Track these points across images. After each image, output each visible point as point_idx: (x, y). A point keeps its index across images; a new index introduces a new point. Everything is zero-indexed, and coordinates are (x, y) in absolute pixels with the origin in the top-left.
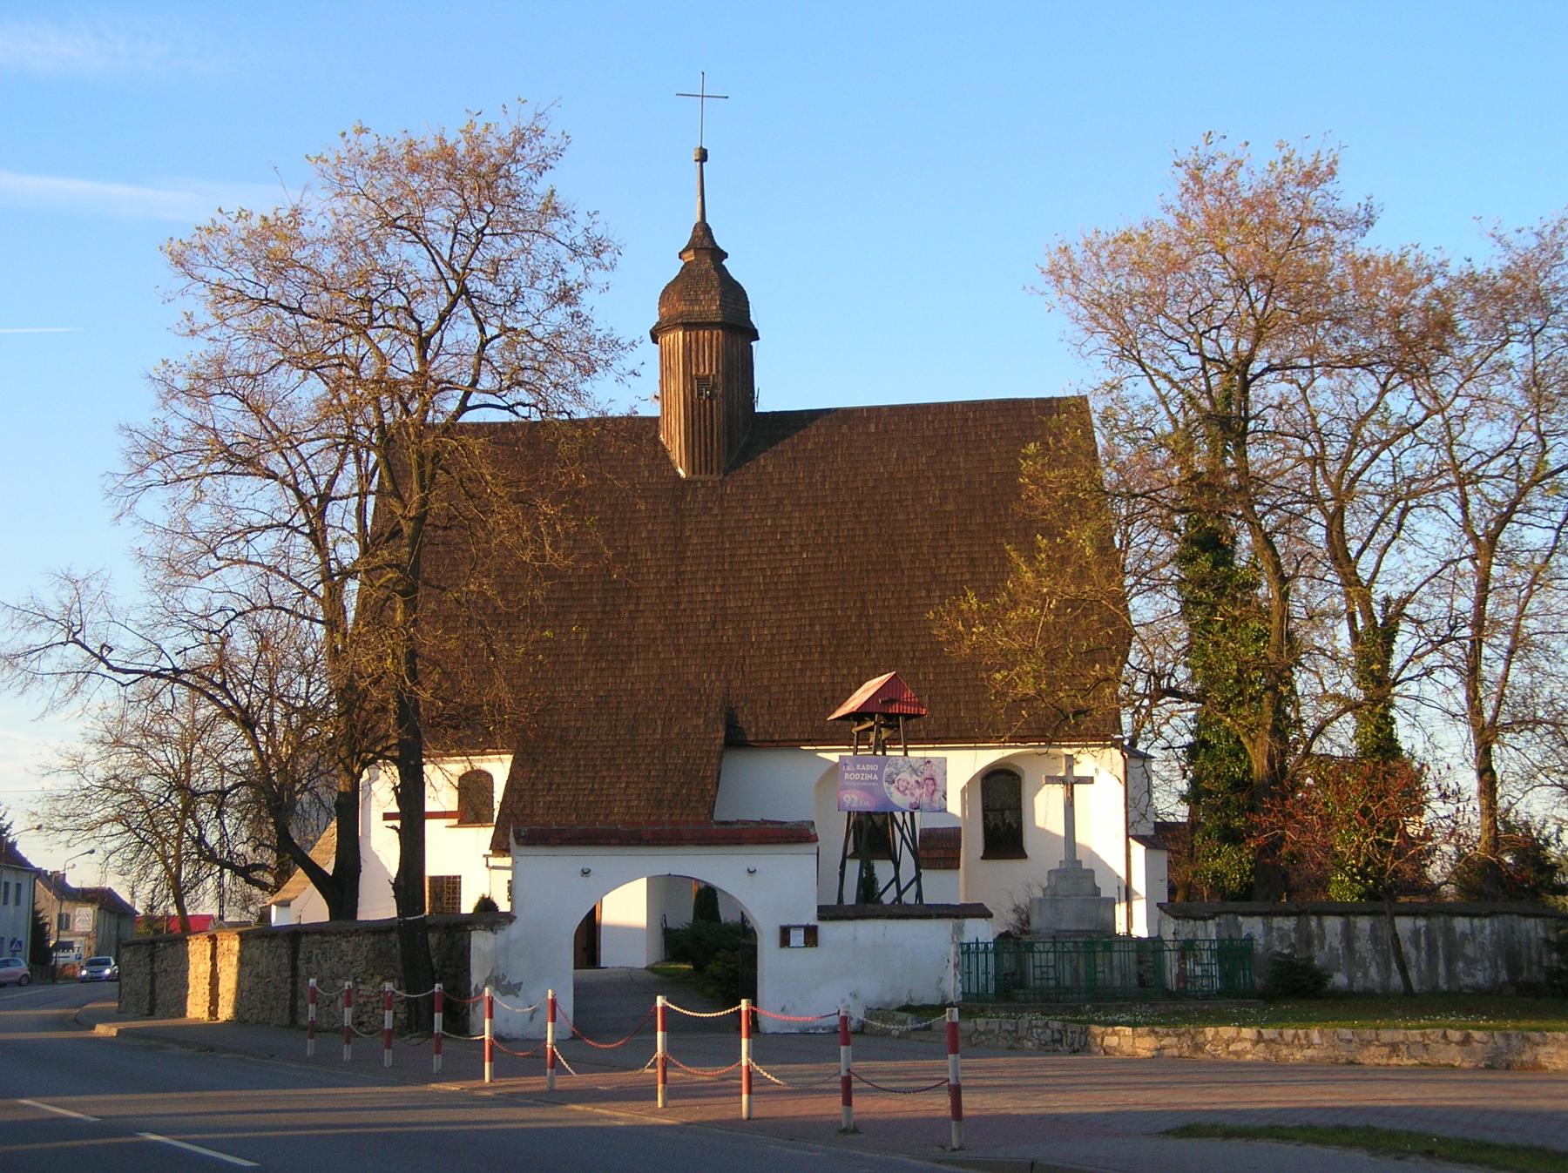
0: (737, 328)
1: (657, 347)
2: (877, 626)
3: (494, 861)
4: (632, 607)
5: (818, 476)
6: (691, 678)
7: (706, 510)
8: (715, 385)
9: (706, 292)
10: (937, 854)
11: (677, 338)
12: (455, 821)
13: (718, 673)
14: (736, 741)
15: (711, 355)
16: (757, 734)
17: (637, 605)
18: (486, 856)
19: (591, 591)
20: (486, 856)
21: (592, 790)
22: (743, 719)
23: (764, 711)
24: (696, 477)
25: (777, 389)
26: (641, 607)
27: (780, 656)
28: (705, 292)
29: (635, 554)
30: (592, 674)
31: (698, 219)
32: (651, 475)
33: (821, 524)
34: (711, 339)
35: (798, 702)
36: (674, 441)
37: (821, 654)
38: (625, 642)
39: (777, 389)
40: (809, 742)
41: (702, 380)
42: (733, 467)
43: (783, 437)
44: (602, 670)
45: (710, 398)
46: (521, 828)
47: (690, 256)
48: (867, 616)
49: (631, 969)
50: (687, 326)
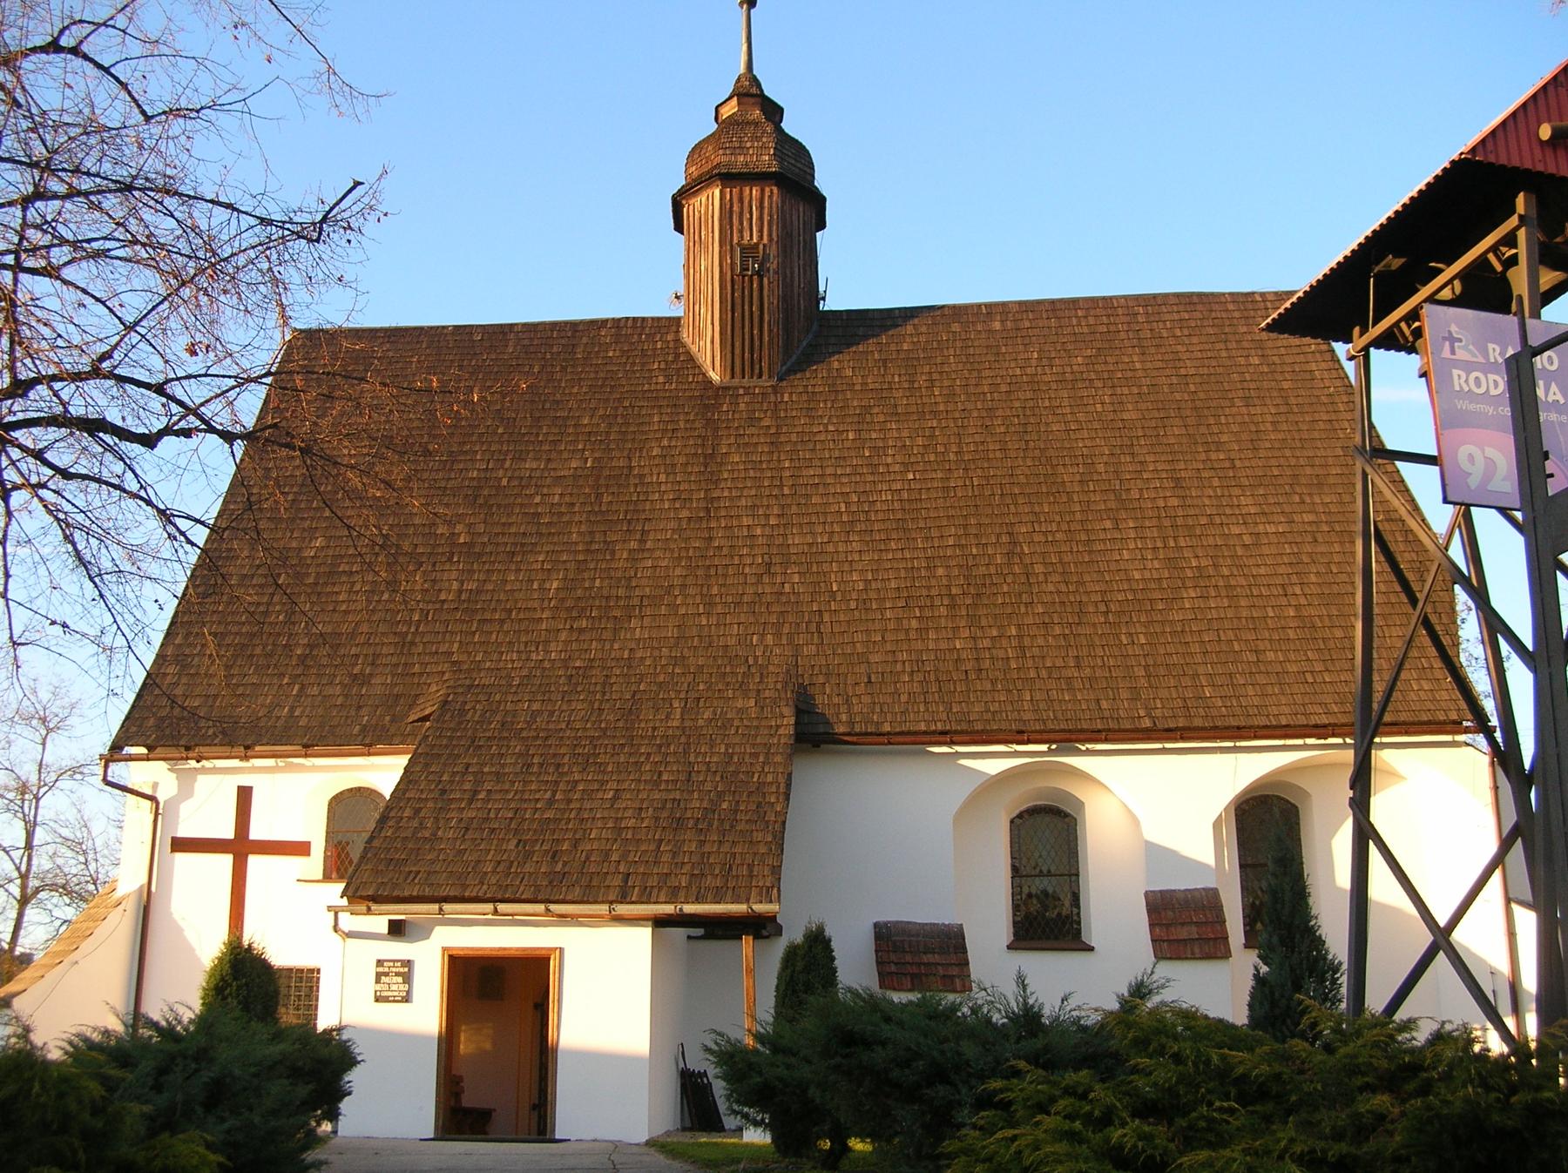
0: (795, 191)
1: (680, 239)
2: (1039, 569)
3: (348, 922)
4: (633, 545)
5: (922, 380)
6: (732, 641)
7: (752, 421)
8: (766, 257)
9: (755, 138)
10: (1183, 933)
11: (711, 200)
12: (700, 932)
13: (778, 635)
14: (815, 736)
15: (761, 218)
16: (851, 723)
17: (642, 541)
18: (335, 911)
19: (569, 523)
20: (335, 911)
21: (551, 801)
22: (823, 701)
23: (860, 689)
24: (736, 382)
25: (851, 276)
26: (649, 545)
27: (882, 610)
28: (752, 139)
29: (642, 476)
30: (563, 636)
31: (742, 69)
32: (669, 380)
33: (932, 436)
34: (760, 200)
35: (918, 677)
36: (706, 348)
37: (952, 606)
38: (621, 592)
39: (851, 276)
40: (948, 736)
41: (749, 251)
42: (792, 371)
43: (866, 337)
44: (581, 631)
45: (760, 274)
46: (380, 863)
47: (730, 110)
48: (1021, 555)
49: (616, 1145)
50: (729, 178)
